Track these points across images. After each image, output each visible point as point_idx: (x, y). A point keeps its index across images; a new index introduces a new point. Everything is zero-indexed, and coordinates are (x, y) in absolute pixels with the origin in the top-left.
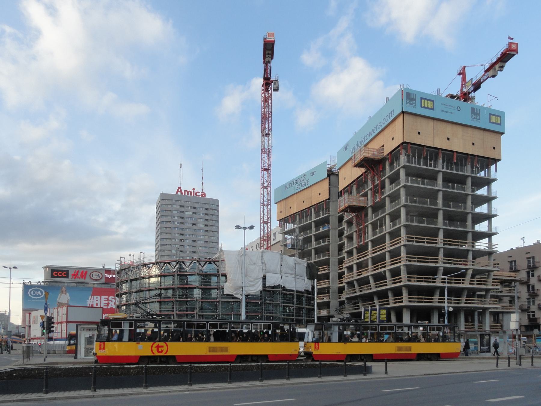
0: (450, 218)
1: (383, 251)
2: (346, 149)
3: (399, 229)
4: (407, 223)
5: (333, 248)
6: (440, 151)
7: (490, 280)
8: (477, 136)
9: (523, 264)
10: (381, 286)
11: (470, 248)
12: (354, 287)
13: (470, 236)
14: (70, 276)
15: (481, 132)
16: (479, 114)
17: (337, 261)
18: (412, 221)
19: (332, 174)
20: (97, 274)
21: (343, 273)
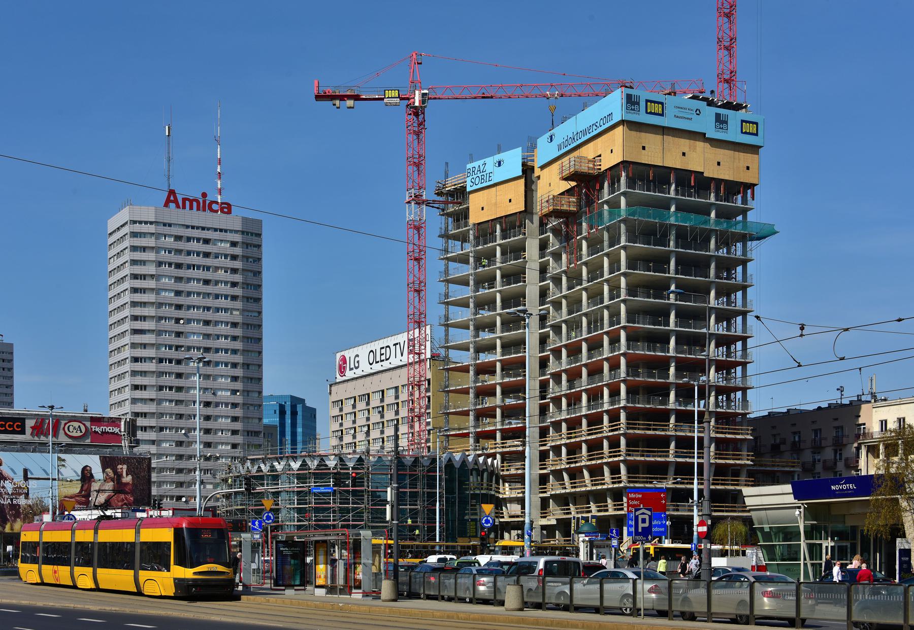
1: (599, 435)
8: (723, 154)
14: (28, 430)
16: (726, 122)
17: (537, 430)
20: (76, 424)
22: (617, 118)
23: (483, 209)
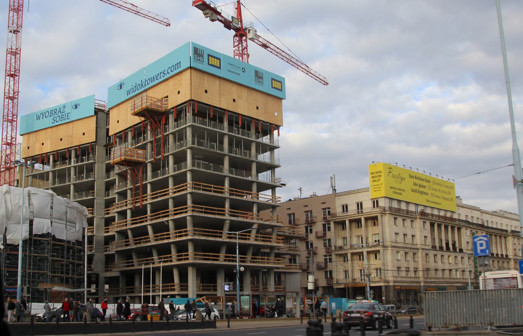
0: (234, 164)
2: (121, 88)
3: (185, 173)
4: (194, 168)
5: (99, 186)
6: (226, 112)
7: (274, 236)
9: (301, 219)
10: (163, 239)
11: (255, 200)
12: (126, 218)
13: (254, 187)
15: (265, 97)
16: (262, 78)
17: (104, 202)
18: (199, 165)
19: (101, 114)
21: (113, 219)
22: (185, 65)
23: (61, 140)
